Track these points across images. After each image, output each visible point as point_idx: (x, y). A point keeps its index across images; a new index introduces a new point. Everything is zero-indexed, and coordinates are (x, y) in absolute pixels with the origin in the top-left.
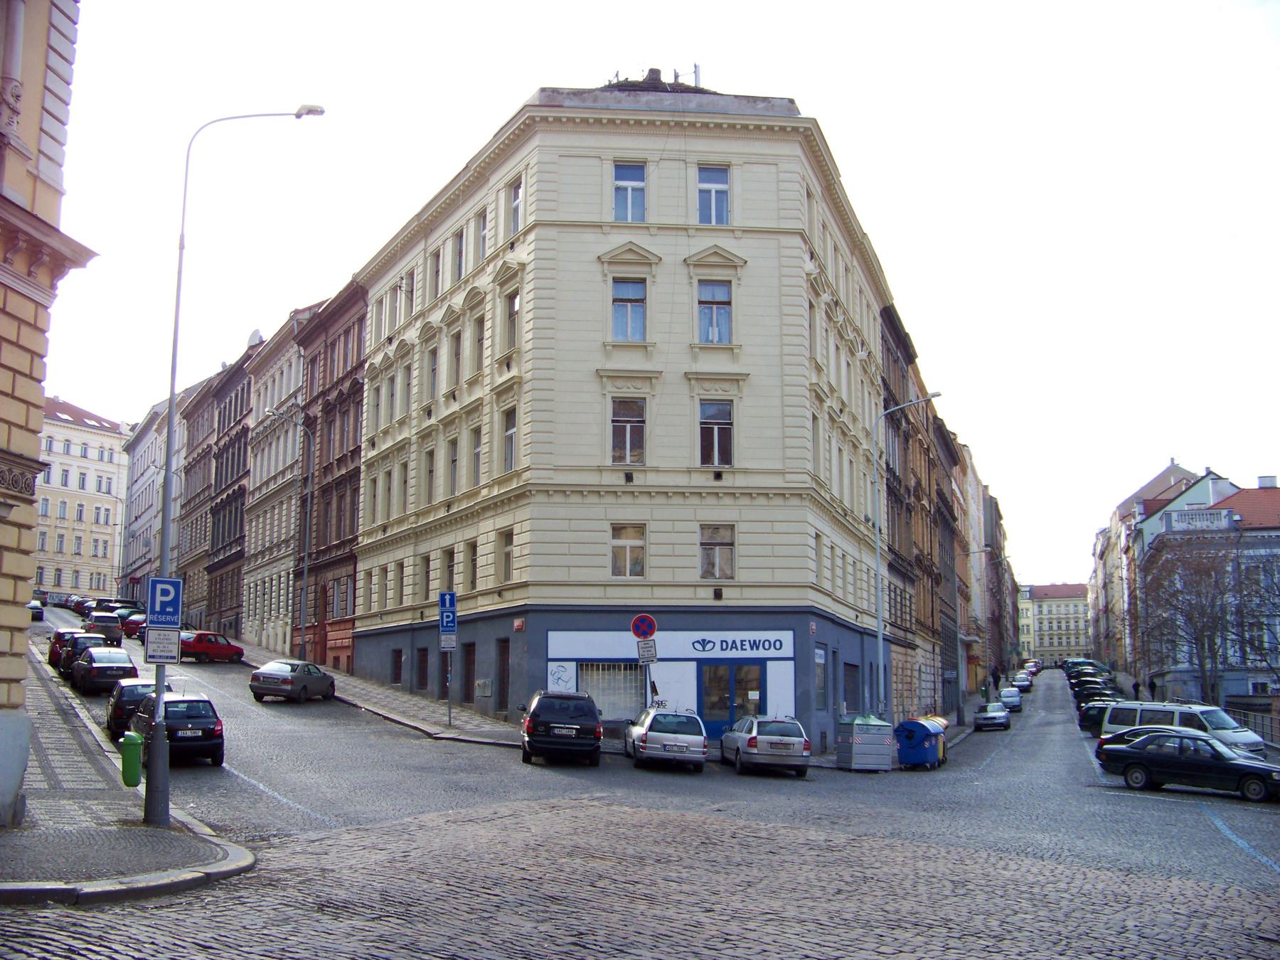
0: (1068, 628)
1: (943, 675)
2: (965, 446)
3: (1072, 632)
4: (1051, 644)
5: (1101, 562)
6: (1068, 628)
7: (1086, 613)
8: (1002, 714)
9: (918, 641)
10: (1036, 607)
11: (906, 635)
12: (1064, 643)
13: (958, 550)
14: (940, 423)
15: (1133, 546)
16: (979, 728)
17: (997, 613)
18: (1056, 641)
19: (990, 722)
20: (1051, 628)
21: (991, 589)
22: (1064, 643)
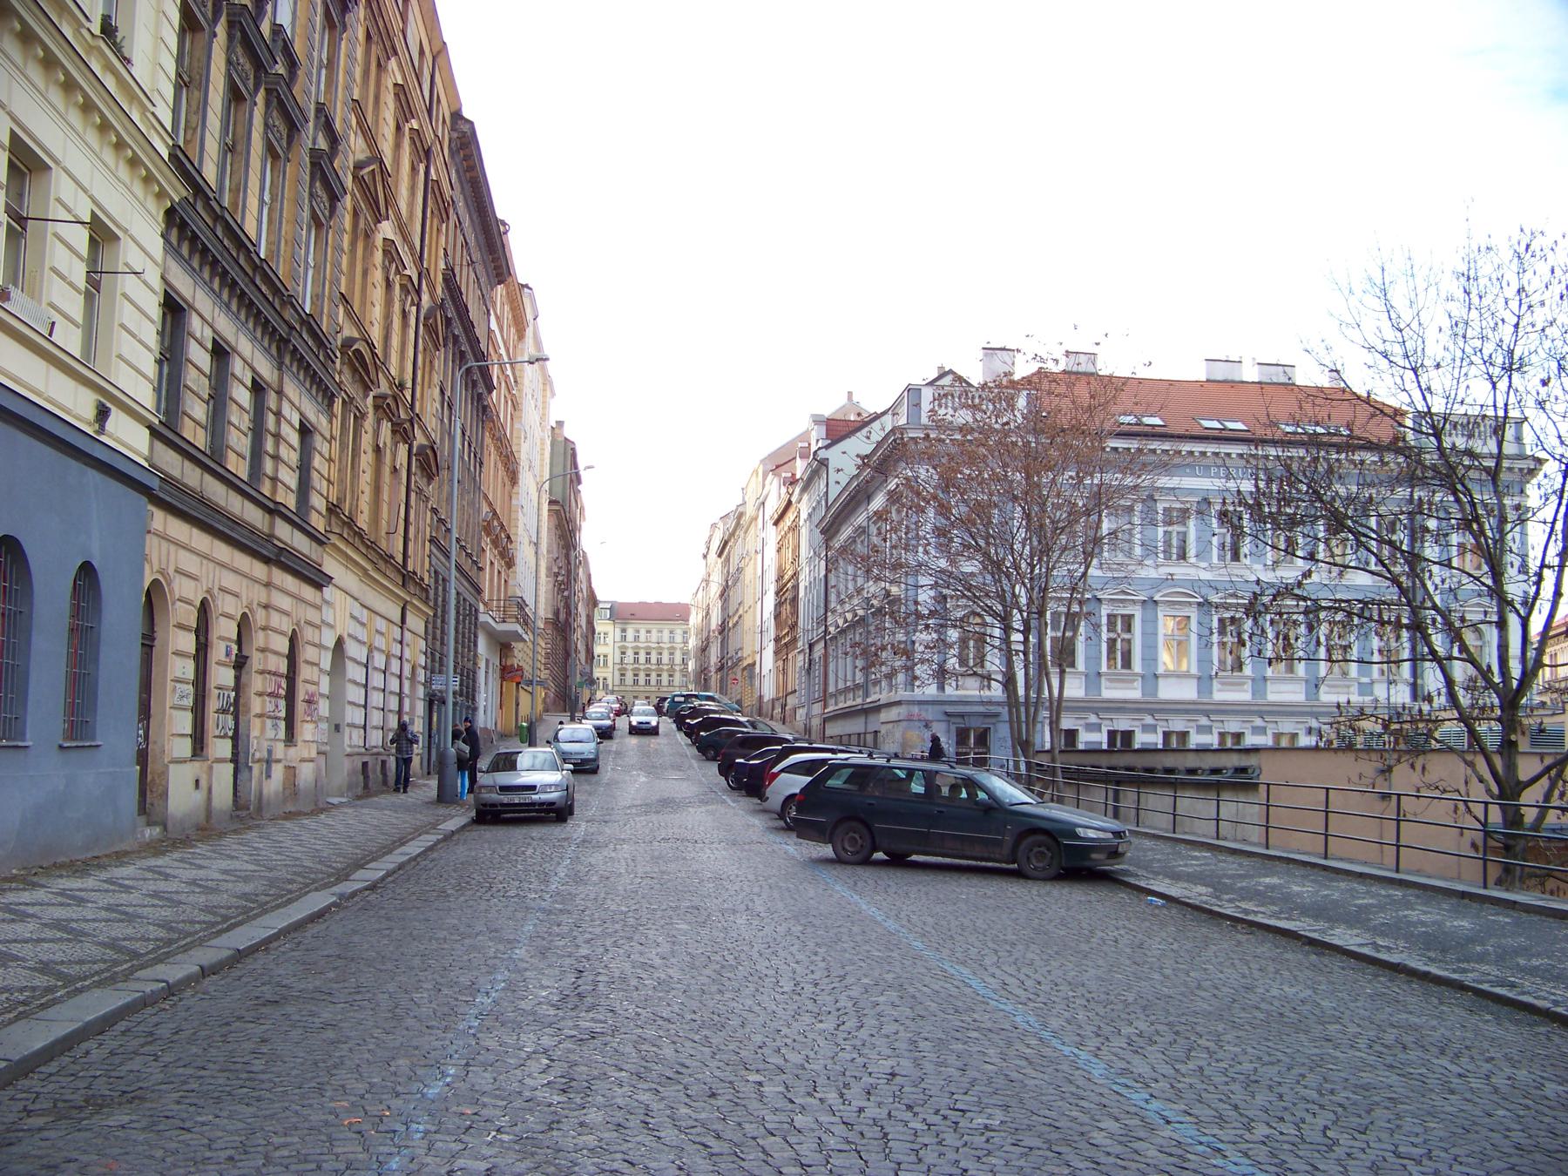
0: (659, 662)
1: (428, 683)
2: (527, 286)
3: (665, 667)
4: (636, 682)
5: (720, 561)
6: (659, 662)
7: (685, 642)
8: (553, 777)
9: (331, 566)
10: (618, 631)
11: (272, 525)
12: (653, 682)
13: (492, 459)
14: (465, 128)
15: (799, 501)
16: (489, 815)
17: (562, 616)
18: (642, 678)
19: (516, 799)
20: (636, 661)
21: (556, 574)
22: (653, 682)
